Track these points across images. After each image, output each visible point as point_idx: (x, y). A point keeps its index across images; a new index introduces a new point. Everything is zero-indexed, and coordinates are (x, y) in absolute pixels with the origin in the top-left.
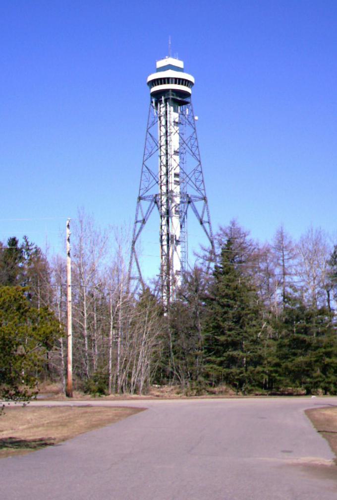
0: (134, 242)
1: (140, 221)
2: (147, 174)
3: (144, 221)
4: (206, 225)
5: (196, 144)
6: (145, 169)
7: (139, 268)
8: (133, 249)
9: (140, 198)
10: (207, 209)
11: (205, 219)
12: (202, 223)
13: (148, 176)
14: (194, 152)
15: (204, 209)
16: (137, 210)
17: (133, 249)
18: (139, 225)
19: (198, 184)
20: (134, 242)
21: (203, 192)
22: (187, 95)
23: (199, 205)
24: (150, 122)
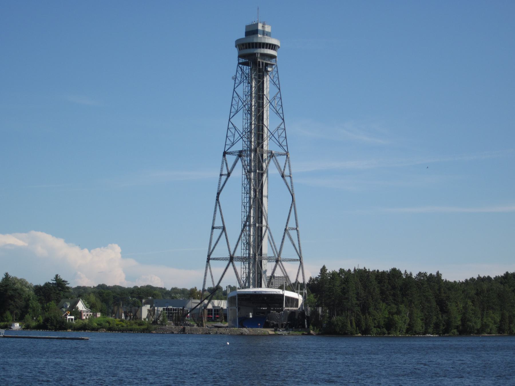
0: (218, 194)
1: (219, 228)
2: (233, 131)
3: (229, 175)
4: (288, 179)
5: (276, 76)
6: (235, 95)
7: (221, 215)
8: (217, 199)
9: (225, 153)
10: (302, 269)
11: (287, 172)
12: (283, 176)
13: (233, 132)
14: (287, 228)
15: (291, 207)
16: (207, 268)
17: (217, 199)
18: (224, 178)
19: (281, 140)
20: (218, 194)
21: (285, 148)
22: (273, 57)
23: (282, 160)
24: (233, 110)
